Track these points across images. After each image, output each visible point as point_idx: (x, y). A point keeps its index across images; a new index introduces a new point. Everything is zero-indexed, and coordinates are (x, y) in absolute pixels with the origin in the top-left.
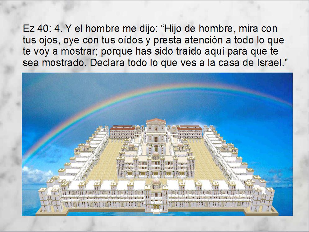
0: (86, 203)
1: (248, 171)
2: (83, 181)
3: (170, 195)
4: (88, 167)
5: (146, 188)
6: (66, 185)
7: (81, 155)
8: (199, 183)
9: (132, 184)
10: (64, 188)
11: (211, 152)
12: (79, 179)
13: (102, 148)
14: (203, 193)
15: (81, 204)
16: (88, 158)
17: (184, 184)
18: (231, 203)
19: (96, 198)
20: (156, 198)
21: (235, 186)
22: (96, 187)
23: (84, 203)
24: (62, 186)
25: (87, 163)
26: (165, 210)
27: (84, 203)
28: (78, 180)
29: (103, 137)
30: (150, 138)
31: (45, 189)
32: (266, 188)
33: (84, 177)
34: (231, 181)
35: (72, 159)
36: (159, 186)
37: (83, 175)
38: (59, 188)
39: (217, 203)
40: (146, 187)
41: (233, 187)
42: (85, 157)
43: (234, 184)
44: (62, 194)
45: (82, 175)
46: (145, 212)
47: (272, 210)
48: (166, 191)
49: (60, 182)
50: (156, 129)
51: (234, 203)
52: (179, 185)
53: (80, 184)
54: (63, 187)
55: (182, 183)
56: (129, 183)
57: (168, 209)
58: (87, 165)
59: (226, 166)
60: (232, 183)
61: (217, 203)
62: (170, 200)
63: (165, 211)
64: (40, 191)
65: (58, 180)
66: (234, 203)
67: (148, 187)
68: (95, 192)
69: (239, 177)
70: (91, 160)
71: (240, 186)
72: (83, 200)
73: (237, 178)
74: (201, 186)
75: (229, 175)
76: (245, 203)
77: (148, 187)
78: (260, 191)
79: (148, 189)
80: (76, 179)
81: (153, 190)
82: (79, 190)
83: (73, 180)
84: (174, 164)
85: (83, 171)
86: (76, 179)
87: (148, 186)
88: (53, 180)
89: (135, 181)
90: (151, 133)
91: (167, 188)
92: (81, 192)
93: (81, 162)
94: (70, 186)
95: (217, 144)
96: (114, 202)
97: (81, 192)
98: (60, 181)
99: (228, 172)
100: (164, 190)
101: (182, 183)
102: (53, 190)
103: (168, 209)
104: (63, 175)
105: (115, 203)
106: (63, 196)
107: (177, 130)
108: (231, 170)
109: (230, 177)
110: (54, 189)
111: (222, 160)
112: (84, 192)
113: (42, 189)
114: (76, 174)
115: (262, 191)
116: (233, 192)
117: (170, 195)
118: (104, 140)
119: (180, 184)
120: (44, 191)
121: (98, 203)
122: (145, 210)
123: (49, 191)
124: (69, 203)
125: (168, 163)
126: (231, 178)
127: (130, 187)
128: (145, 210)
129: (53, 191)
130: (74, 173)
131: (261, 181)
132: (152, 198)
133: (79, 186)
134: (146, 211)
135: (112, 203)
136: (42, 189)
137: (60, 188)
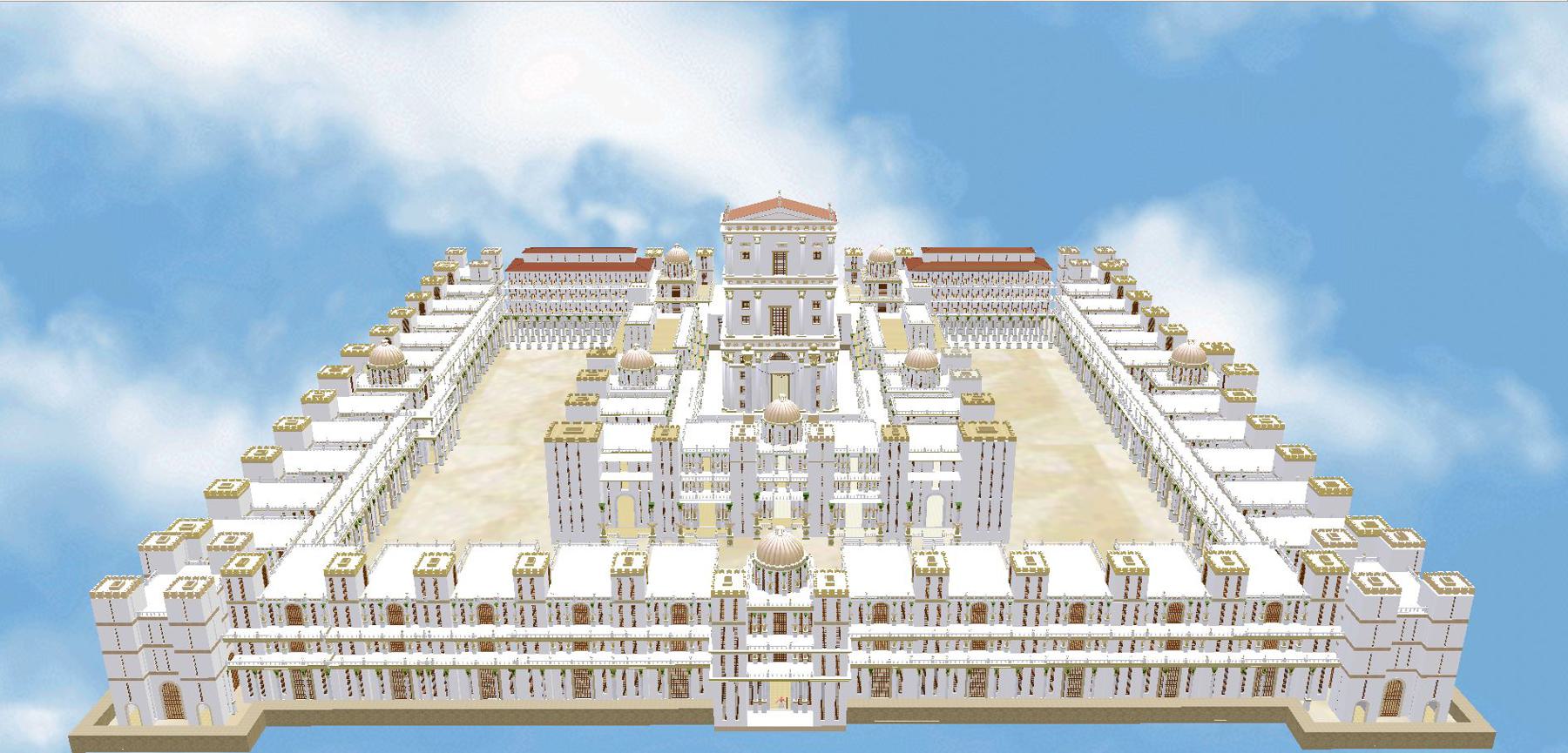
0: (369, 675)
1: (1320, 492)
2: (351, 549)
3: (857, 630)
4: (381, 476)
5: (719, 587)
6: (249, 567)
7: (317, 439)
8: (1030, 560)
9: (638, 564)
10: (241, 583)
11: (1101, 393)
12: (330, 538)
13: (464, 375)
14: (1053, 617)
15: (337, 678)
16: (380, 425)
17: (940, 564)
18: (1221, 671)
19: (424, 645)
20: (779, 642)
21: (1242, 574)
22: (429, 581)
23: (358, 674)
24: (226, 574)
25: (373, 454)
26: (829, 710)
27: (358, 674)
28: (319, 541)
29: (457, 329)
30: (746, 312)
31: (129, 583)
32: (1424, 575)
33: (366, 525)
34: (1216, 548)
35: (287, 429)
36: (795, 576)
37: (355, 518)
38: (212, 581)
39: (1137, 672)
40: (720, 578)
41: (1233, 580)
42: (362, 417)
43: (1238, 565)
44: (229, 620)
45: (348, 518)
46: (717, 724)
47: (1455, 712)
48: (831, 611)
49: (217, 548)
50: (779, 260)
51: (1235, 674)
52: (915, 571)
53: (335, 566)
54: (235, 583)
55: (931, 560)
56: (621, 560)
57: (850, 710)
58: (367, 471)
59: (1189, 469)
60: (1226, 560)
61: (1137, 672)
62: (859, 657)
63: (830, 720)
64: (100, 595)
65: (205, 541)
66: (1235, 674)
67: (728, 579)
68: (420, 608)
69: (1265, 524)
70: (402, 441)
71: (1271, 578)
72: (349, 659)
73: (1251, 536)
74: (1042, 575)
75: (1205, 517)
76: (1299, 677)
77: (728, 579)
78: (1391, 591)
79: (731, 589)
80: (309, 537)
81: (757, 598)
82: (328, 596)
83: (295, 543)
84: (817, 629)
85: (350, 500)
86: (309, 541)
87: (733, 575)
88: (173, 539)
89: (656, 549)
90: (747, 281)
91: (840, 584)
92: (341, 608)
93: (341, 446)
94: (271, 578)
95: (1136, 347)
96: (535, 667)
97: (341, 608)
98: (220, 542)
99: (1200, 503)
100: (823, 597)
101: (931, 560)
102: (178, 588)
103: (850, 710)
104: (326, 418)
105: (536, 673)
106: (231, 632)
107: (902, 274)
108: (1217, 493)
109: (1215, 530)
110: (183, 583)
111: (1169, 442)
112: (357, 611)
113: (110, 583)
114: (371, 443)
115: (1399, 591)
116: (1229, 607)
117: (857, 630)
118: (477, 327)
119: (922, 563)
120: (124, 595)
121: (439, 673)
122: (710, 711)
123: (153, 598)
124: (269, 677)
125: (770, 617)
126: (1220, 538)
127: (628, 580)
128: (710, 711)
129: (174, 595)
130: (296, 504)
131: (1396, 540)
132: (755, 642)
133: (330, 575)
134: (719, 721)
135: (522, 675)
136: (110, 583)
137: (217, 577)
